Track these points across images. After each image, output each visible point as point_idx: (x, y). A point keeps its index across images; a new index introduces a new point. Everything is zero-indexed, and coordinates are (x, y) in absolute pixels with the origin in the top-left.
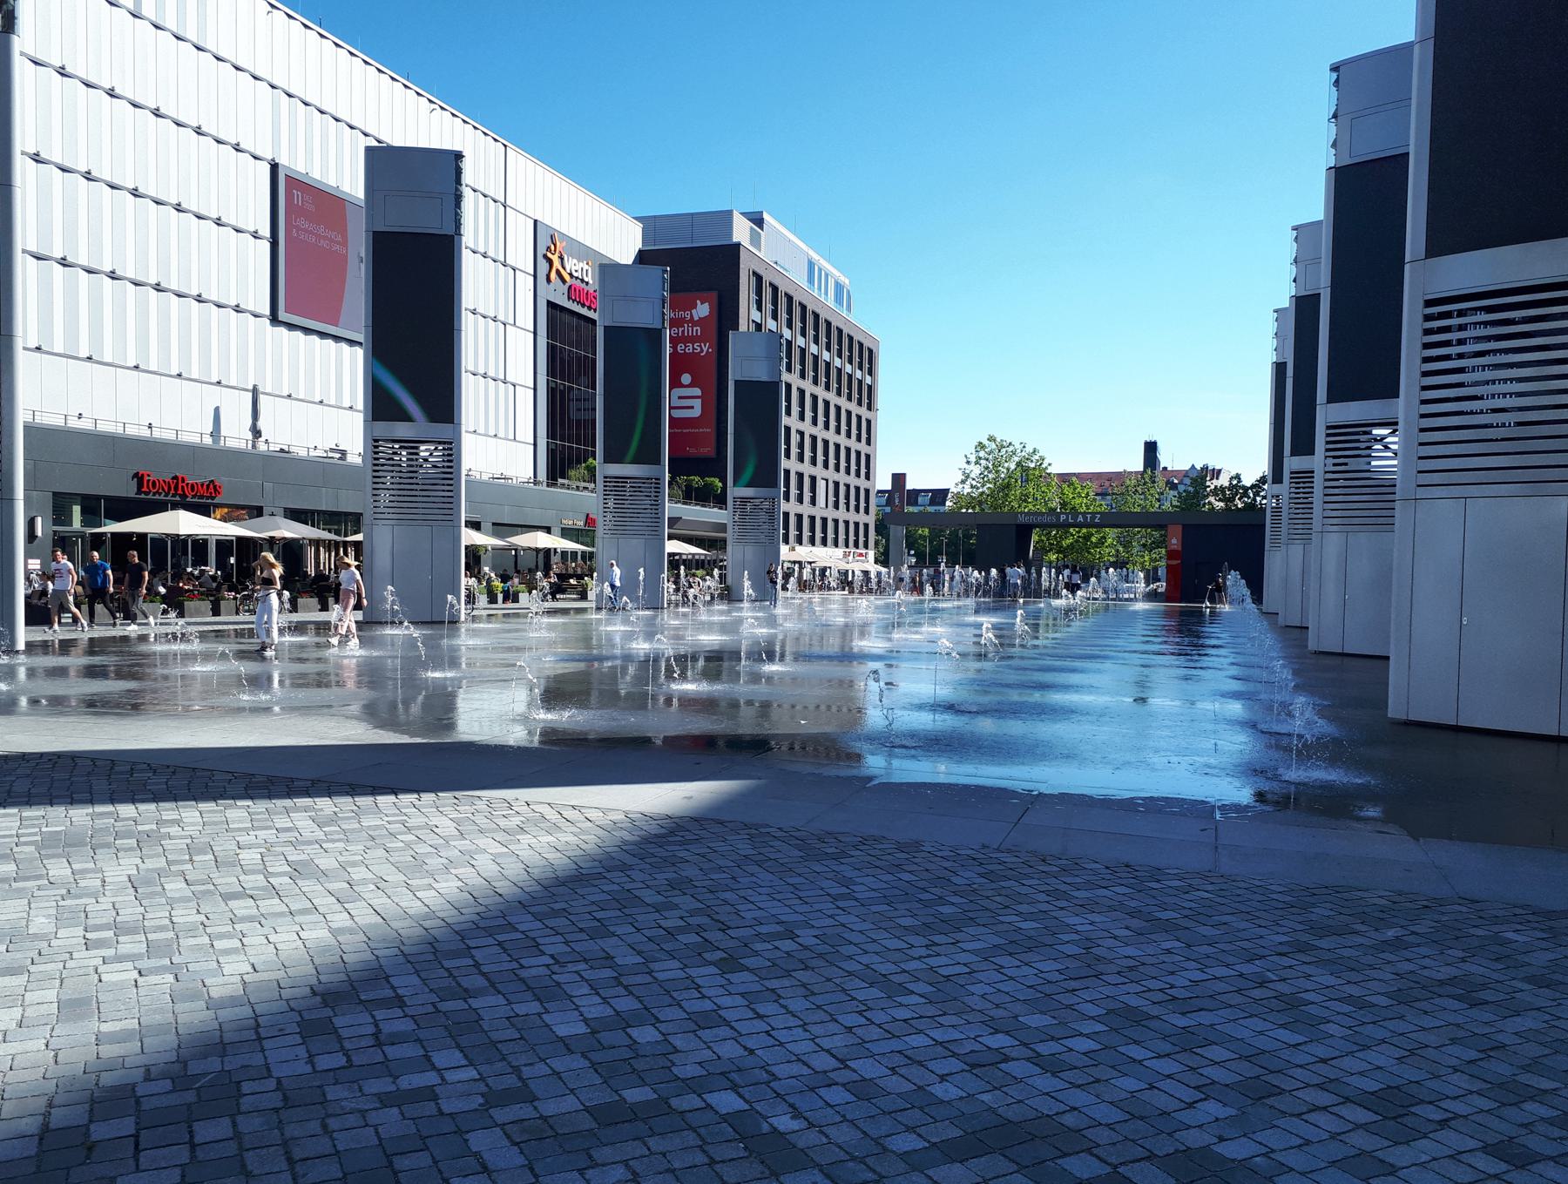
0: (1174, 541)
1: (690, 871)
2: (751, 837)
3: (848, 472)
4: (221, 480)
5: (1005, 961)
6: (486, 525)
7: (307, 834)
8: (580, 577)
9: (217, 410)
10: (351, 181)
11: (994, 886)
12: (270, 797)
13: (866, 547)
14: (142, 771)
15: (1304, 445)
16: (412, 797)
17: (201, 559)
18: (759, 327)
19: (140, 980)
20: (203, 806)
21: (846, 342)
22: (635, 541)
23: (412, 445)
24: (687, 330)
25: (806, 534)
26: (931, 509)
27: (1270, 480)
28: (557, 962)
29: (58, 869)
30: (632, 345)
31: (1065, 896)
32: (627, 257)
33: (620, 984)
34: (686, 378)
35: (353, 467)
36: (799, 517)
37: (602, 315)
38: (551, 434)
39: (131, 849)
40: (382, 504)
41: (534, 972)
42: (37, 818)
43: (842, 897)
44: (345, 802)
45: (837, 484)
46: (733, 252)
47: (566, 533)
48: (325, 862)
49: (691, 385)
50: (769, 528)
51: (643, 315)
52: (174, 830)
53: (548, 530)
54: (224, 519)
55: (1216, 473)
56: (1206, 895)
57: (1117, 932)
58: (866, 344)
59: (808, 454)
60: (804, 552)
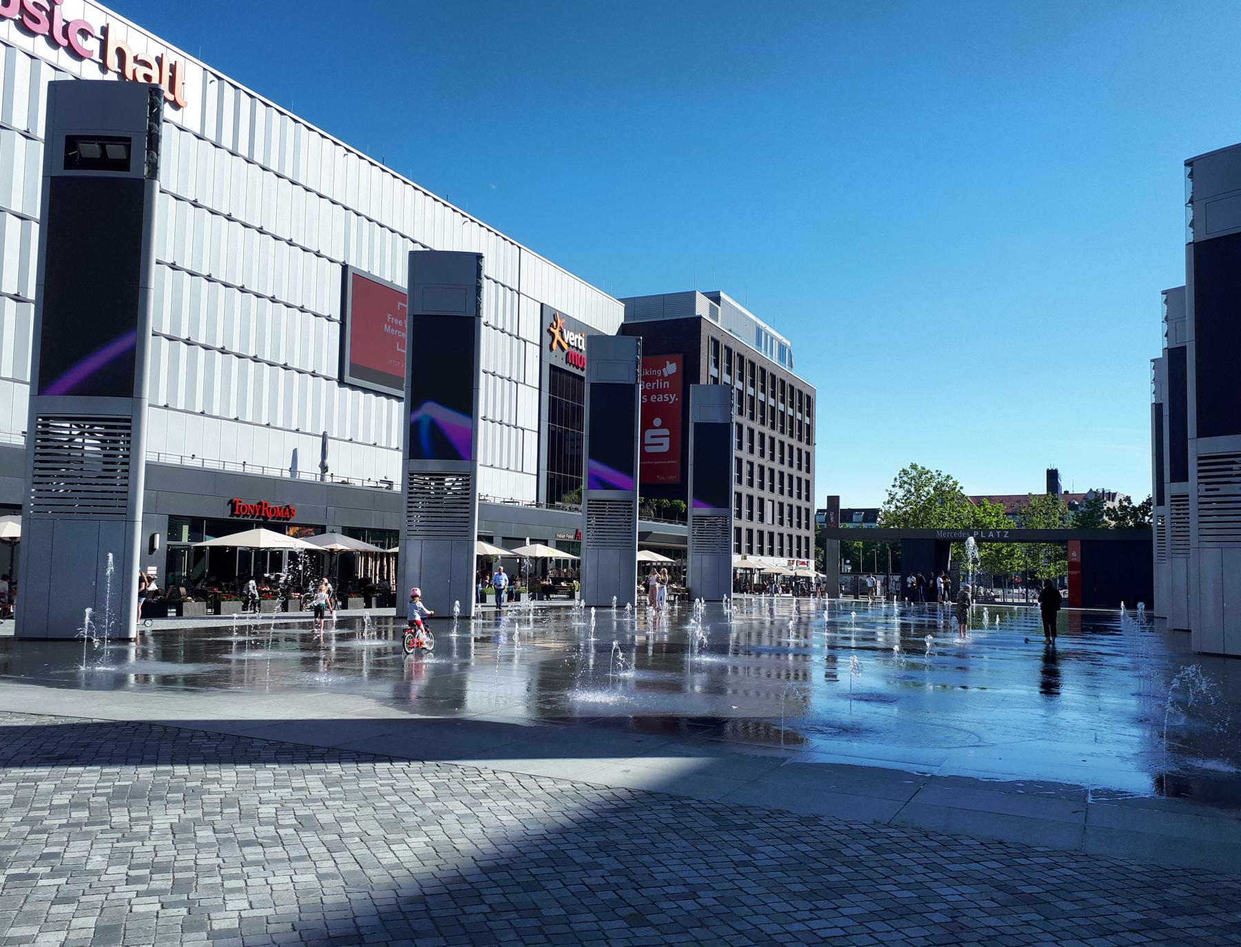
0: (1074, 554)
1: (618, 836)
2: (674, 807)
3: (799, 497)
4: (296, 505)
5: (878, 926)
6: (498, 539)
7: (315, 793)
8: (569, 580)
9: (295, 451)
10: (399, 277)
11: (878, 858)
12: (293, 762)
13: (807, 556)
14: (200, 737)
15: (1180, 474)
16: (403, 765)
17: (277, 567)
18: (716, 380)
19: (161, 912)
20: (240, 768)
21: (788, 390)
22: (611, 552)
23: (439, 477)
24: (659, 384)
25: (756, 545)
26: (865, 525)
27: (1154, 501)
28: (493, 910)
29: (120, 817)
30: (613, 399)
31: (941, 868)
32: (611, 329)
33: (542, 932)
34: (657, 422)
35: (395, 494)
36: (750, 532)
37: (589, 373)
38: (551, 466)
39: (177, 802)
40: (414, 524)
41: (472, 918)
42: (112, 774)
43: (745, 864)
44: (351, 768)
45: (781, 505)
46: (696, 323)
47: (560, 545)
48: (325, 817)
49: (663, 426)
50: (720, 541)
51: (620, 375)
52: (214, 787)
53: (546, 543)
54: (295, 536)
55: (1112, 496)
56: (1069, 872)
57: (982, 903)
58: (805, 392)
59: (756, 480)
60: (754, 561)
